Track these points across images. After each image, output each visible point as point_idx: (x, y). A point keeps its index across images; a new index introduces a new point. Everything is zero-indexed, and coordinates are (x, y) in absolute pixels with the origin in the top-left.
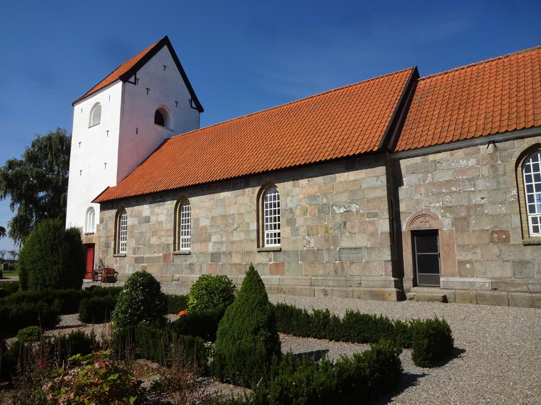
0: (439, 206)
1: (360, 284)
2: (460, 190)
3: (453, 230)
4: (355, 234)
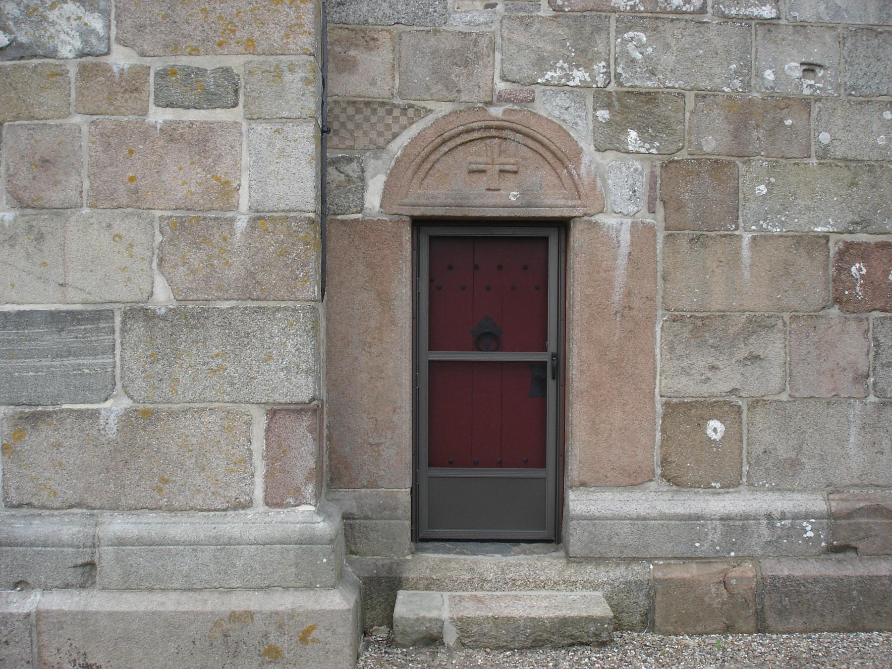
0: (585, 86)
1: (91, 565)
2: (703, 10)
3: (651, 228)
4: (59, 211)
